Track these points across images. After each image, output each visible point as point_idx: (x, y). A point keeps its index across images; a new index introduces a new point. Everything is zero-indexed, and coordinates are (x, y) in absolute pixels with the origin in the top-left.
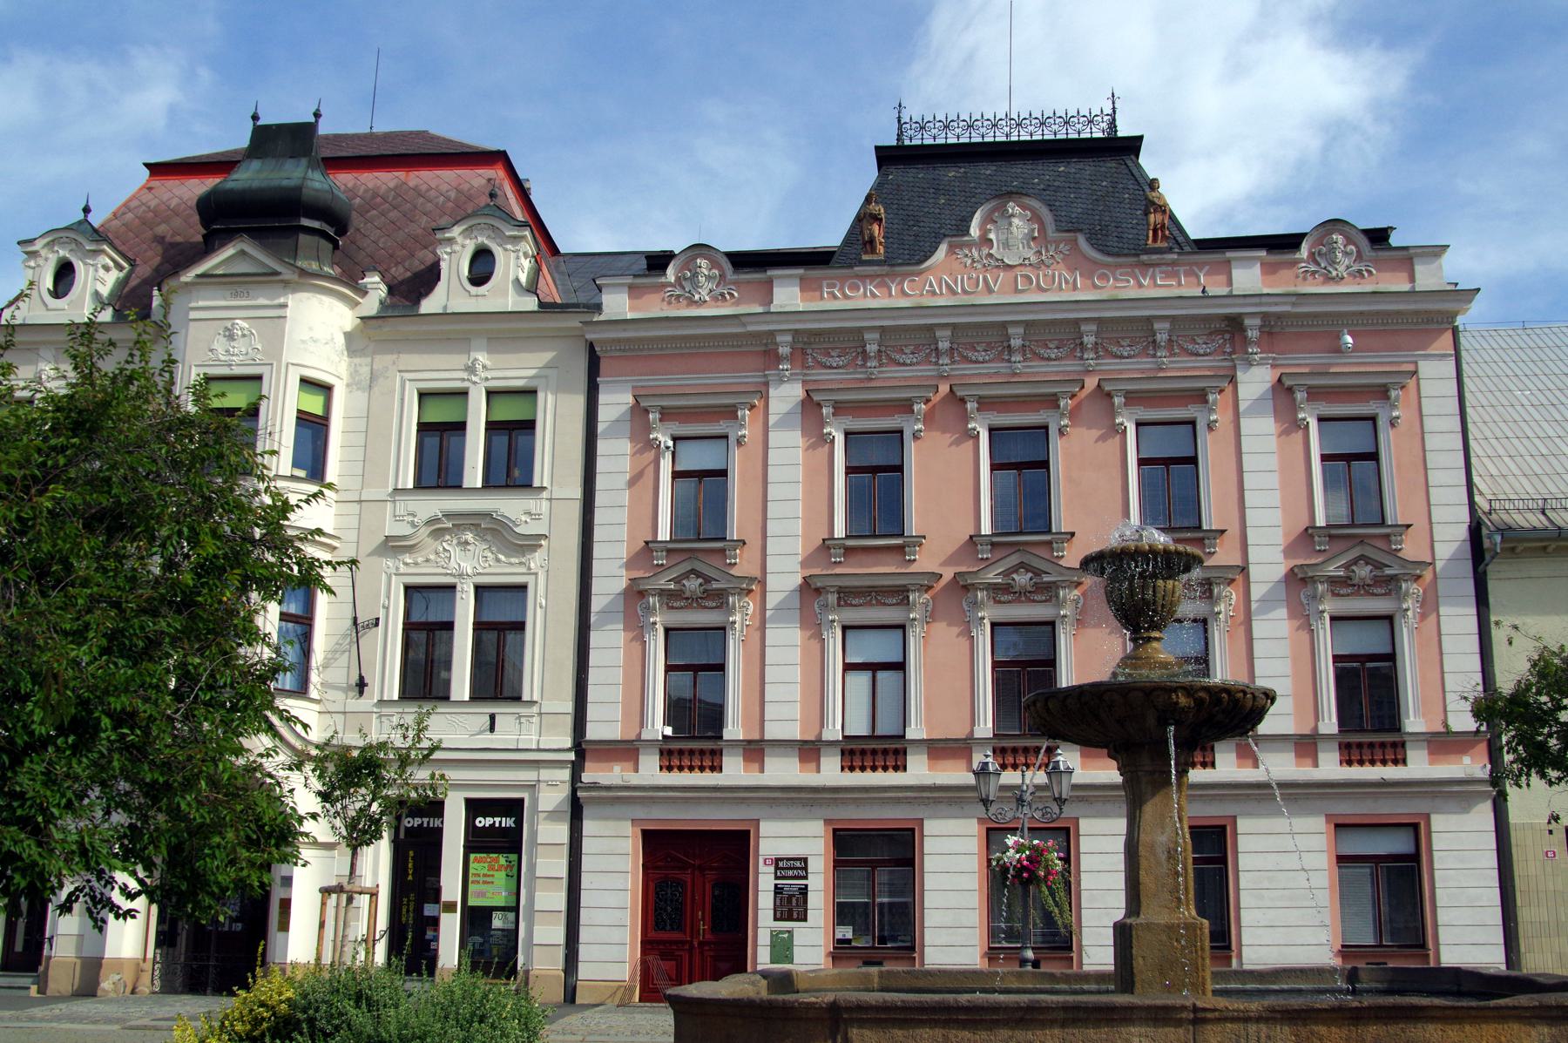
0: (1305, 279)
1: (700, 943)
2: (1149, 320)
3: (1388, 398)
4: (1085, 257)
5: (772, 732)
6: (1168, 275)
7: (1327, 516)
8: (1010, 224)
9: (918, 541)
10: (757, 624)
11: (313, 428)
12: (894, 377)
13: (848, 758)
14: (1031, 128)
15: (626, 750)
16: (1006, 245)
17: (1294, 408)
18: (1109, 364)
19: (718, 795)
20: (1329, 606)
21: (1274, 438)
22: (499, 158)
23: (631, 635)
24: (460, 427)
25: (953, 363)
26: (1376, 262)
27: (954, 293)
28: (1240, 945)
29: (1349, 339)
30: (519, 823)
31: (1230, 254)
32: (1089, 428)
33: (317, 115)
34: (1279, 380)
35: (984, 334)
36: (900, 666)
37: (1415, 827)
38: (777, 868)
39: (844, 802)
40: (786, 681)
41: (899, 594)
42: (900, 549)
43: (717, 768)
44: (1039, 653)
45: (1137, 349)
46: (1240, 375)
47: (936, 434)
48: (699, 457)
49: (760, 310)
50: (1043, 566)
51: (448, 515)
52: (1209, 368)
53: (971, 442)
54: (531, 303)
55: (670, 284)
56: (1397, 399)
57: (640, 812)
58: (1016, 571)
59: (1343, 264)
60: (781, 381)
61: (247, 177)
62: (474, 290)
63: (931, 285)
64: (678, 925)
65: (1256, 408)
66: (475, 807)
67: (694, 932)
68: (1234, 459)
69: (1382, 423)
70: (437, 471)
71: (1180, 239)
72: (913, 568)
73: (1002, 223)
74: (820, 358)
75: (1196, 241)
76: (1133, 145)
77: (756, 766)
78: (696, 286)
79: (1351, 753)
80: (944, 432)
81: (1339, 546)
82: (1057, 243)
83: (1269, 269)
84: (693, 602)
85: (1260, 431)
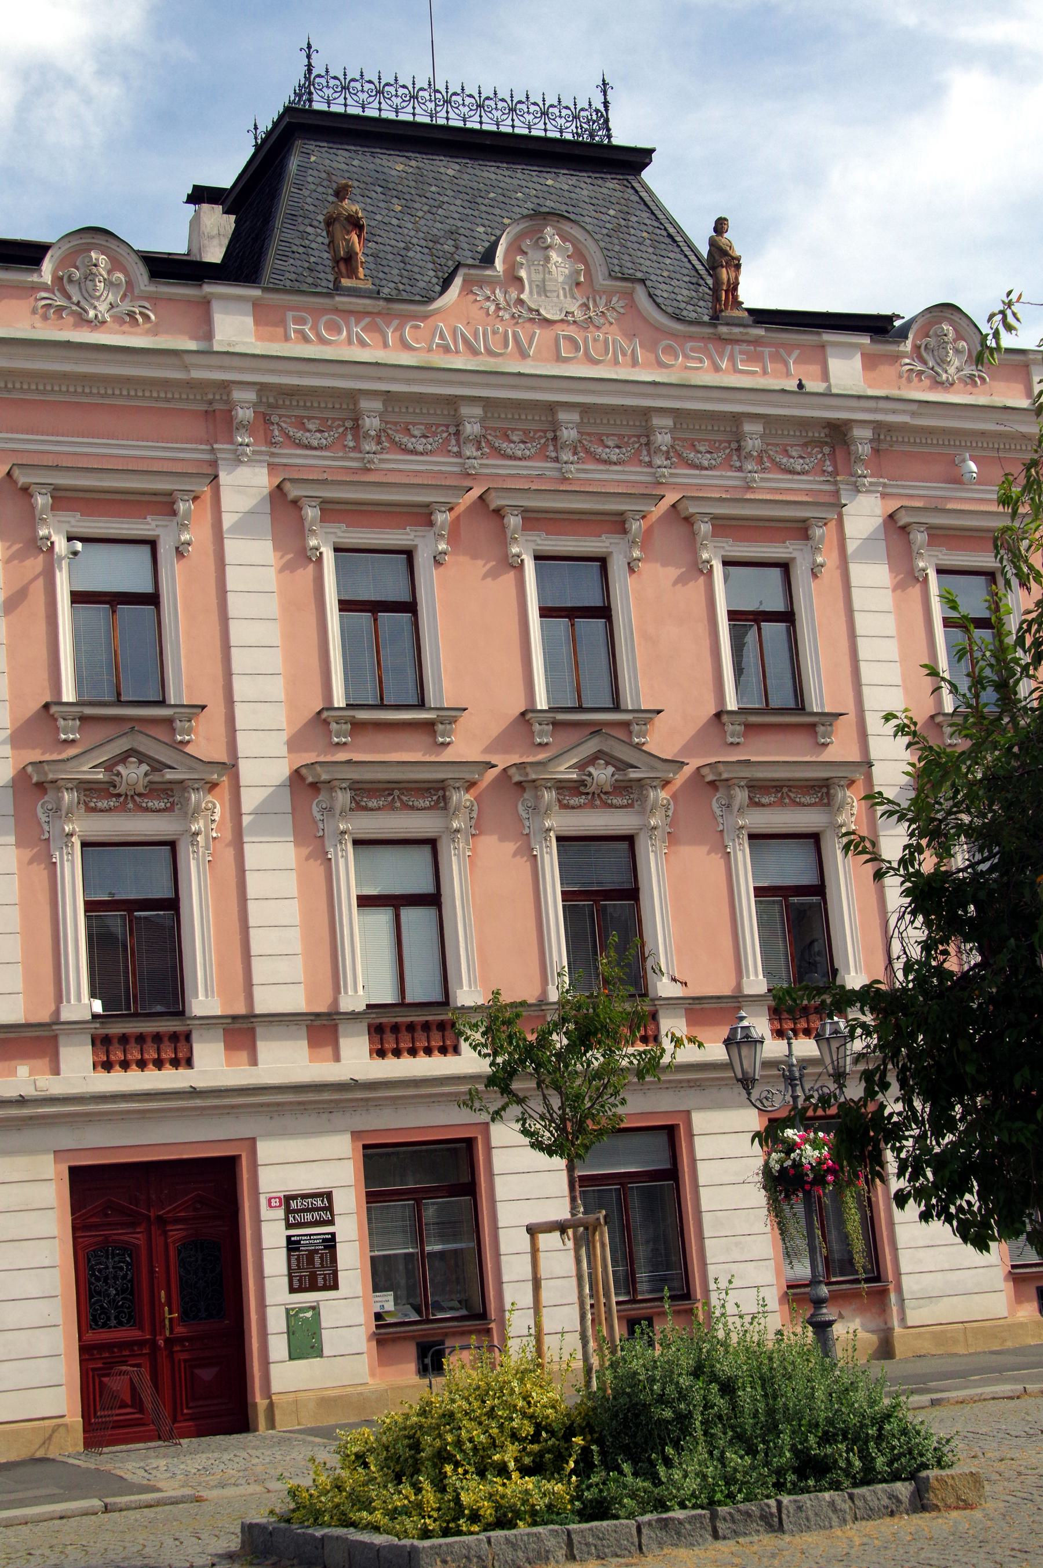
0: (909, 380)
1: (167, 1341)
2: (737, 418)
3: (174, 513)
4: (645, 320)
5: (266, 1002)
6: (752, 358)
7: (347, 697)
8: (547, 259)
9: (453, 715)
10: (228, 835)
12: (610, 478)
14: (329, 92)
16: (542, 289)
17: (301, 530)
18: (686, 476)
19: (198, 1102)
20: (81, 826)
21: (890, 591)
23: (28, 854)
25: (764, 470)
26: (154, 299)
27: (475, 352)
28: (898, 1274)
29: (973, 467)
31: (828, 337)
32: (664, 564)
35: (530, 419)
36: (433, 900)
37: (670, 1132)
38: (288, 1211)
39: (378, 1104)
40: (277, 924)
41: (435, 793)
42: (429, 726)
44: (612, 879)
45: (627, 452)
46: (225, 478)
47: (463, 559)
48: (122, 571)
49: (192, 345)
50: (163, 755)
52: (808, 492)
53: (702, 580)
55: (44, 287)
56: (188, 514)
57: (68, 1139)
59: (955, 365)
60: (238, 461)
63: (442, 337)
64: (130, 1316)
65: (245, 527)
67: (156, 1327)
68: (843, 619)
69: (165, 550)
72: (447, 755)
73: (535, 255)
74: (398, 437)
75: (751, 312)
76: (637, 159)
77: (328, 1051)
78: (90, 296)
79: (110, 1049)
80: (475, 557)
81: (570, 737)
82: (610, 294)
83: (870, 362)
84: (130, 801)
85: (873, 579)
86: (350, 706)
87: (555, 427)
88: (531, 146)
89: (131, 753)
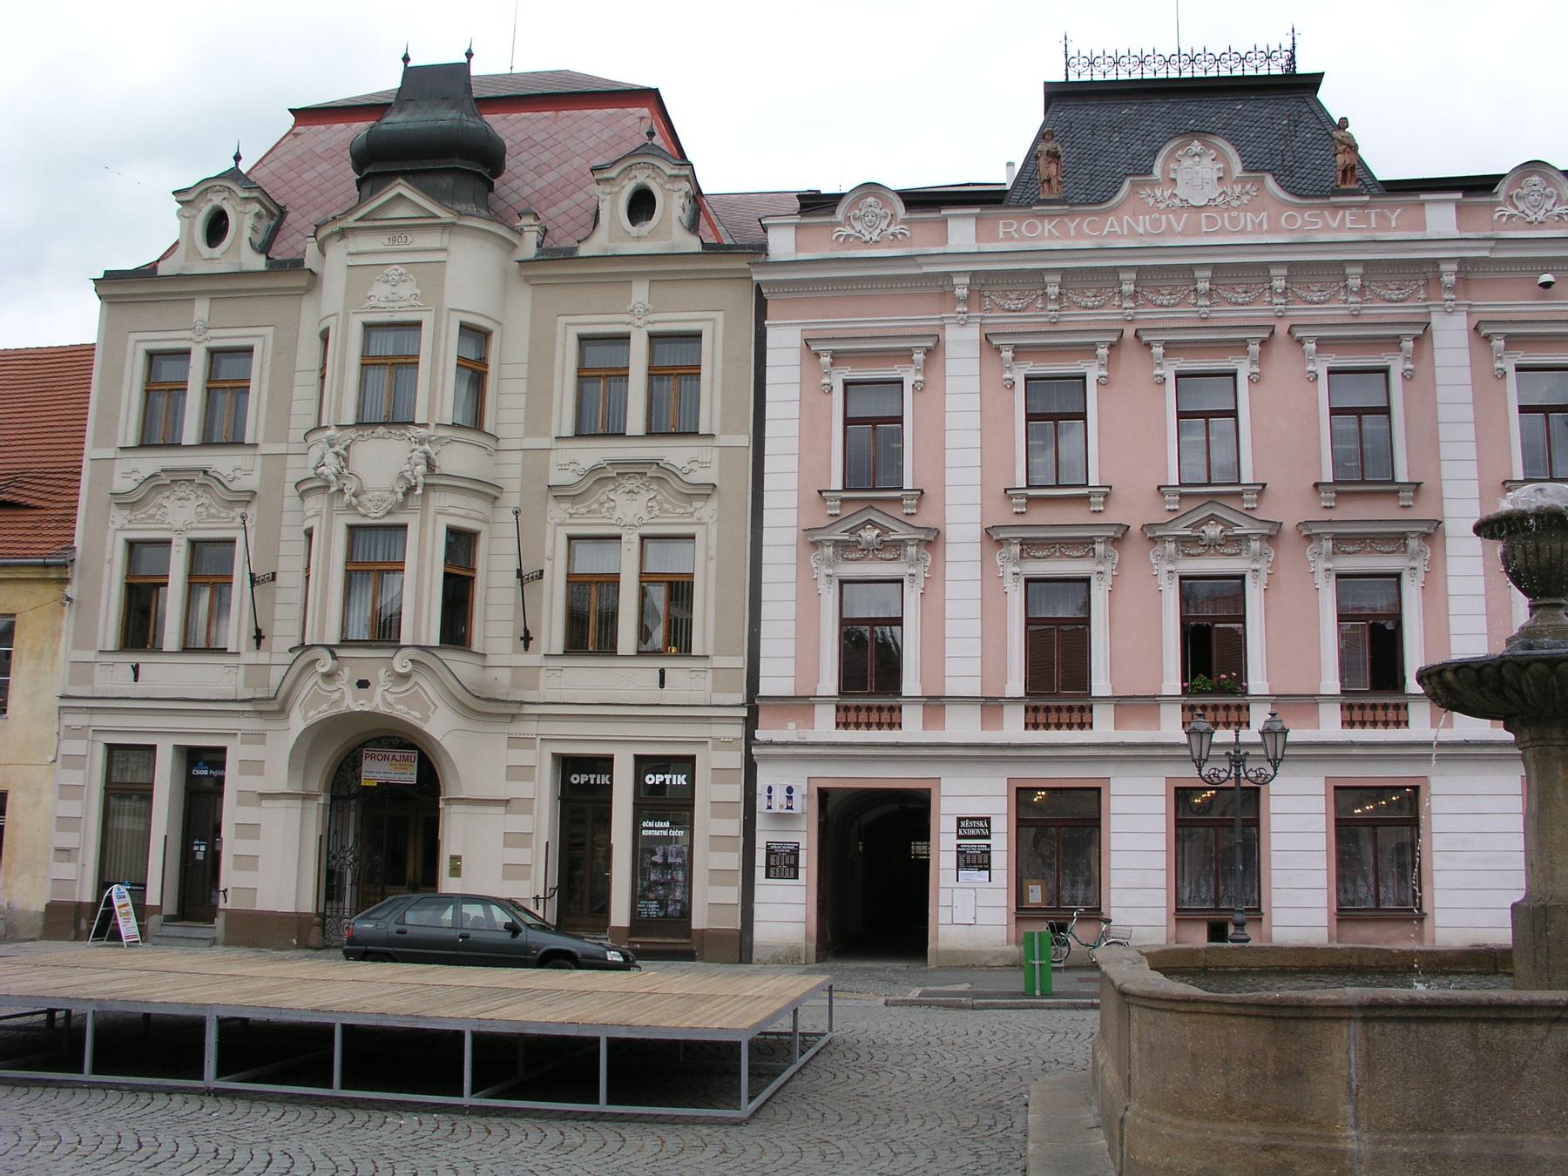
5: (953, 687)
11: (475, 373)
13: (1347, 713)
14: (1080, 68)
15: (800, 704)
22: (651, 97)
24: (622, 374)
30: (611, 779)
33: (469, 55)
34: (1476, 329)
43: (1401, 723)
51: (613, 464)
54: (694, 245)
58: (1206, 523)
61: (397, 121)
62: (634, 230)
66: (644, 764)
70: (597, 422)
71: (1368, 181)
76: (1314, 80)
84: (1213, 547)
86: (1336, 482)
87: (1439, 275)
88: (1146, 86)
89: (1212, 517)
